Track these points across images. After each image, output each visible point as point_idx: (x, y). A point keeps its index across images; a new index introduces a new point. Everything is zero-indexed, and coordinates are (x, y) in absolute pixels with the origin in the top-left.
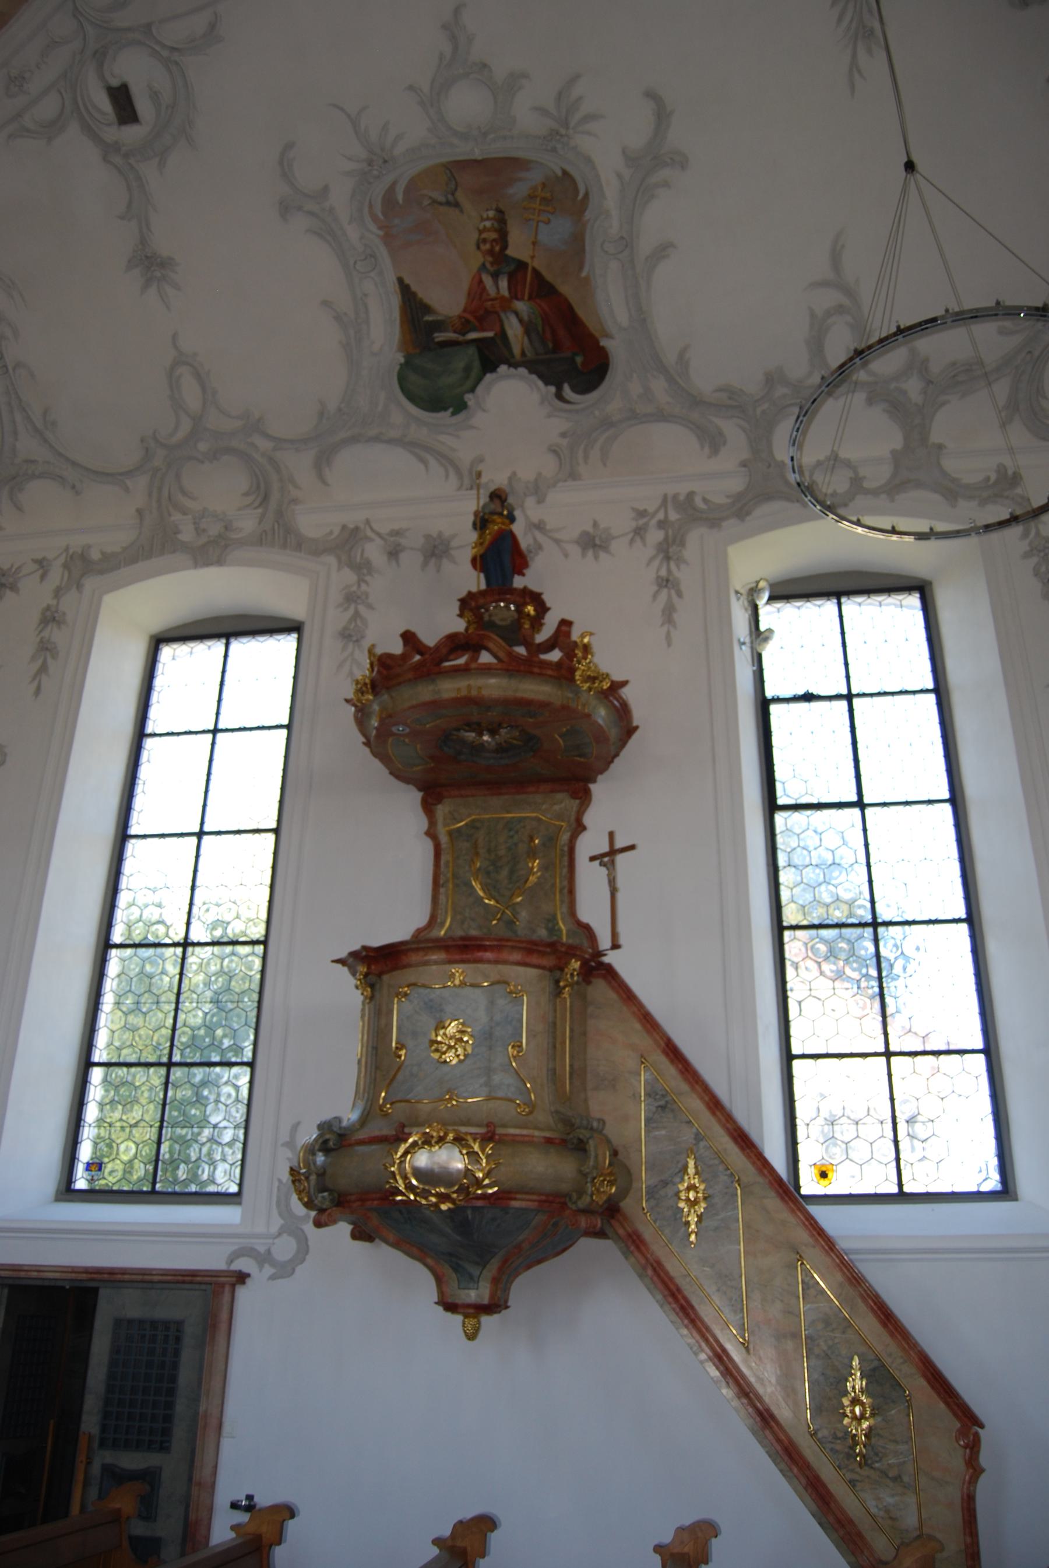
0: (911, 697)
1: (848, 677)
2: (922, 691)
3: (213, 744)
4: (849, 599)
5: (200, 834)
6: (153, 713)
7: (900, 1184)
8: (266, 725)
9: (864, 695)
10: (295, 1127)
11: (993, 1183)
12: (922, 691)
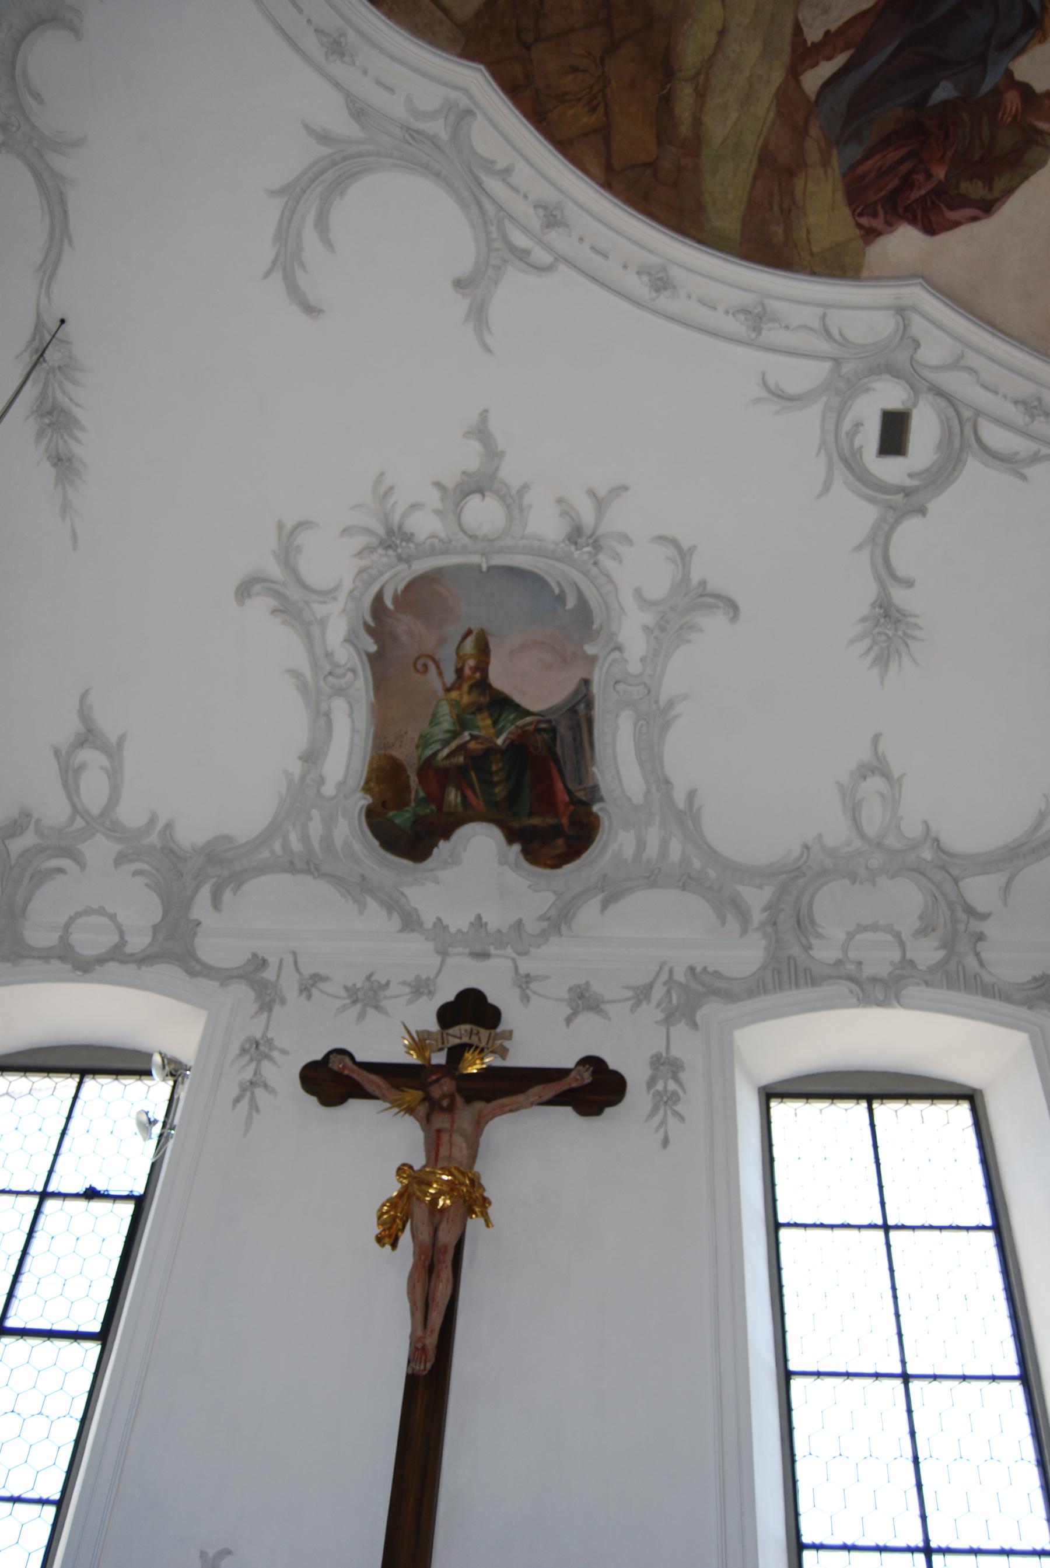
0: (827, 1232)
3: (38, 1212)
5: (906, 1378)
9: (903, 1227)
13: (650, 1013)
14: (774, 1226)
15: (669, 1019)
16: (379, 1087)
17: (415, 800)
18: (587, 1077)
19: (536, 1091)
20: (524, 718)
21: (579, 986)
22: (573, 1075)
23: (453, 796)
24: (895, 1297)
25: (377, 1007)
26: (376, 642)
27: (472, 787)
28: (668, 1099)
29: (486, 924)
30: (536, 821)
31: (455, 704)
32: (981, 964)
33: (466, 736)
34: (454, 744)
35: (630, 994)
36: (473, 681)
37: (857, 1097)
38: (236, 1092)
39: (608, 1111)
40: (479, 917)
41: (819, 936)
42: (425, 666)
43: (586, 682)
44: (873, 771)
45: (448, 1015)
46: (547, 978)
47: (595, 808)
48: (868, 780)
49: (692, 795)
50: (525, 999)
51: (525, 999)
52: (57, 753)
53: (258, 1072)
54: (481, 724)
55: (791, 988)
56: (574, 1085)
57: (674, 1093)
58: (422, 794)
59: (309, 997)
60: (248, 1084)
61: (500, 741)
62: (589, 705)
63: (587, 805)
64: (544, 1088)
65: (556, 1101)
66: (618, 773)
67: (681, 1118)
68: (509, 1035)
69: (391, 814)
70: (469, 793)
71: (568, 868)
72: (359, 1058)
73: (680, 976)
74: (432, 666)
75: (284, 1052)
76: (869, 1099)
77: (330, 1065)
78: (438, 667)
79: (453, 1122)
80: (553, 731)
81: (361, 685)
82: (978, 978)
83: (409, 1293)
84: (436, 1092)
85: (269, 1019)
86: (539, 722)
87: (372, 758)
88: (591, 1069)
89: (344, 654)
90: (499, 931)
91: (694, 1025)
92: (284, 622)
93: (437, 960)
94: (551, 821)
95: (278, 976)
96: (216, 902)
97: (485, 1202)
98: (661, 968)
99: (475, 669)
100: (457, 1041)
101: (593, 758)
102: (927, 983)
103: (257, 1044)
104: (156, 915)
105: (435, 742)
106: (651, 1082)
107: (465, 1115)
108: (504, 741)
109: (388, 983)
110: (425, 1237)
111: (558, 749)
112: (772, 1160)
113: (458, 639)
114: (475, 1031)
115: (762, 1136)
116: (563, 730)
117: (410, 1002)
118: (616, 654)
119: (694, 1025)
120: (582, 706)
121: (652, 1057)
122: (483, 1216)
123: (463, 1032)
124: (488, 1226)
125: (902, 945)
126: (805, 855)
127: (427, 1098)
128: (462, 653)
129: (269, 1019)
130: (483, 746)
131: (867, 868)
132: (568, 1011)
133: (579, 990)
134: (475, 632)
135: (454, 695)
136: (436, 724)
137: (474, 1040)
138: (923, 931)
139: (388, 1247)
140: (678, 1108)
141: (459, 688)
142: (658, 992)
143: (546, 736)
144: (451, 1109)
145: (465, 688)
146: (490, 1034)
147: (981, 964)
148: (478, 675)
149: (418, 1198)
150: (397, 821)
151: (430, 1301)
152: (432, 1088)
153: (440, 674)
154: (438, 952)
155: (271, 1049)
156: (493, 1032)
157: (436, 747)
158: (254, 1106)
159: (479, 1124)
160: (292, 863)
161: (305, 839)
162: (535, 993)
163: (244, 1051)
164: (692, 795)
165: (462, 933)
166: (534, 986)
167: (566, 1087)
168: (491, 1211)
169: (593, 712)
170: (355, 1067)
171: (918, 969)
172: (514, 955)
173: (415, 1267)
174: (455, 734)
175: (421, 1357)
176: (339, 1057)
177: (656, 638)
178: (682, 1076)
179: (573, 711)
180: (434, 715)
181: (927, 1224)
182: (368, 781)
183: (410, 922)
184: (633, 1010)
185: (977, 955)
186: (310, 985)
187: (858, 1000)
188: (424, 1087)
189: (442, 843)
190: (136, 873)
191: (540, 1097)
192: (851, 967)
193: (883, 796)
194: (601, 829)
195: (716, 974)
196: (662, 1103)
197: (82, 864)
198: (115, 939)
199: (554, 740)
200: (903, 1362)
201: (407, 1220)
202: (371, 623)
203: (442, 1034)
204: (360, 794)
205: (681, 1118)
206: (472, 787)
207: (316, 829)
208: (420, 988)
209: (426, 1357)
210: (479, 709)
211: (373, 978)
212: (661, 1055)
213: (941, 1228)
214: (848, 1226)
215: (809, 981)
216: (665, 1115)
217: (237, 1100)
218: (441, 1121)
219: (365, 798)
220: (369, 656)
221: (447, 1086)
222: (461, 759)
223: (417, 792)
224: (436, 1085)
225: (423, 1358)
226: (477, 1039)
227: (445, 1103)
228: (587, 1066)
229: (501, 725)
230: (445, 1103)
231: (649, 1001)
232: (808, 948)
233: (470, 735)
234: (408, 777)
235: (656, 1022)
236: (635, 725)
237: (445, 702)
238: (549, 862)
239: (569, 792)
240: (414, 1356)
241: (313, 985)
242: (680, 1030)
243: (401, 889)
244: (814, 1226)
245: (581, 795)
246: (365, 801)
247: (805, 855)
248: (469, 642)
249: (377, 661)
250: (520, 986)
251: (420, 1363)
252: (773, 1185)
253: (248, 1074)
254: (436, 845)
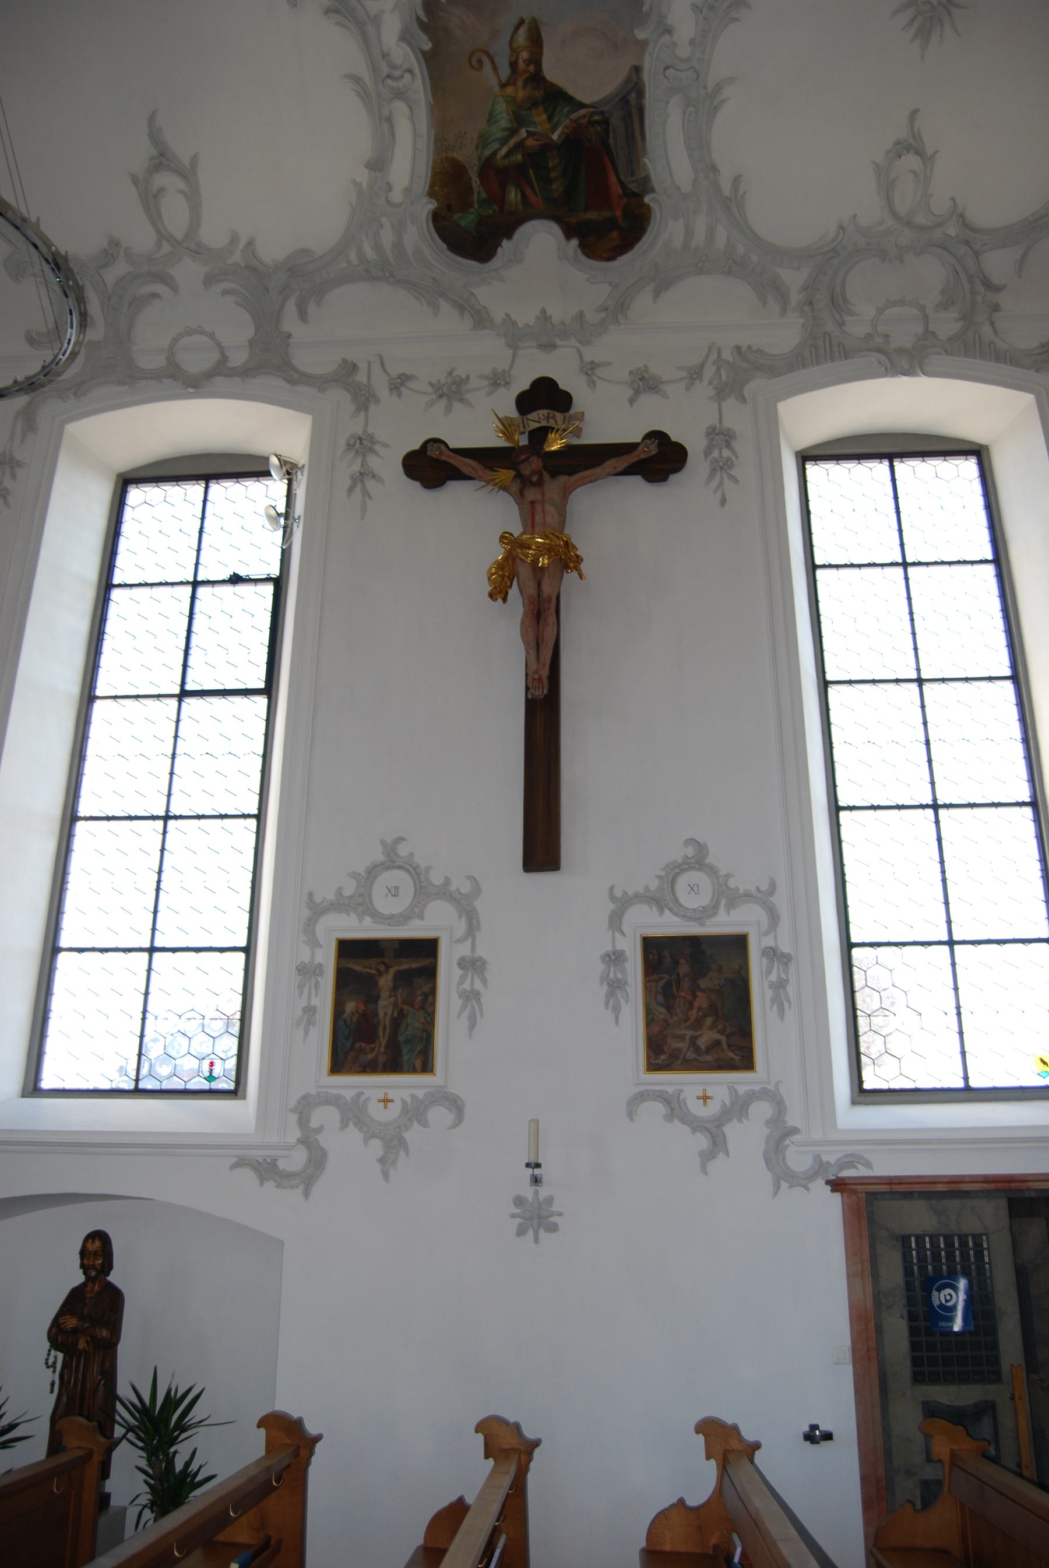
0: (856, 570)
1: (902, 545)
2: (981, 562)
4: (924, 461)
5: (920, 681)
6: (122, 560)
7: (966, 1078)
8: (833, 563)
9: (920, 564)
10: (790, 1007)
11: (870, 1082)
12: (981, 562)
13: (704, 390)
14: (812, 567)
15: (721, 393)
16: (474, 469)
17: (477, 202)
18: (653, 449)
19: (611, 464)
20: (578, 110)
21: (639, 369)
22: (641, 447)
23: (513, 195)
24: (912, 620)
25: (461, 400)
26: (430, 39)
27: (530, 185)
28: (724, 464)
29: (551, 317)
30: (592, 215)
31: (511, 100)
32: (995, 332)
33: (523, 133)
34: (512, 142)
35: (684, 374)
36: (526, 76)
37: (879, 456)
38: (348, 482)
39: (673, 478)
40: (544, 311)
41: (851, 313)
42: (480, 62)
43: (637, 70)
44: (908, 148)
45: (526, 402)
46: (609, 364)
47: (647, 199)
48: (903, 158)
49: (737, 180)
50: (592, 384)
51: (592, 384)
52: (135, 179)
53: (365, 464)
54: (537, 119)
55: (826, 362)
56: (643, 456)
57: (729, 459)
58: (484, 195)
59: (400, 395)
60: (358, 474)
61: (555, 137)
62: (641, 94)
63: (639, 196)
64: (618, 460)
65: (628, 471)
66: (668, 163)
67: (736, 481)
68: (581, 416)
69: (456, 217)
70: (528, 191)
71: (622, 260)
72: (451, 446)
73: (727, 355)
74: (486, 61)
75: (386, 445)
76: (891, 457)
77: (429, 453)
78: (493, 62)
79: (543, 494)
80: (606, 123)
81: (418, 86)
82: (992, 345)
83: (522, 636)
84: (526, 470)
85: (367, 417)
86: (592, 114)
87: (435, 162)
88: (657, 441)
89: (403, 55)
90: (562, 323)
91: (743, 399)
92: (339, 24)
93: (510, 352)
94: (607, 214)
95: (369, 378)
96: (303, 315)
97: (579, 559)
98: (710, 349)
99: (528, 62)
100: (537, 425)
101: (644, 149)
102: (947, 352)
103: (360, 439)
104: (250, 332)
105: (494, 141)
106: (708, 452)
107: (553, 487)
108: (560, 136)
109: (468, 377)
110: (532, 591)
111: (611, 142)
112: (808, 513)
113: (511, 30)
114: (551, 415)
115: (800, 493)
116: (616, 121)
117: (490, 393)
118: (667, 37)
119: (743, 399)
120: (634, 95)
121: (708, 428)
122: (577, 570)
123: (541, 416)
124: (581, 578)
125: (926, 317)
126: (841, 236)
127: (519, 475)
128: (515, 46)
129: (367, 417)
130: (539, 143)
131: (897, 246)
132: (631, 392)
133: (639, 372)
134: (527, 22)
135: (510, 90)
136: (495, 122)
137: (552, 423)
138: (944, 305)
139: (500, 601)
140: (732, 472)
141: (514, 84)
142: (709, 371)
143: (599, 128)
144: (540, 484)
145: (520, 83)
146: (565, 417)
147: (995, 332)
148: (532, 68)
149: (521, 560)
150: (462, 223)
151: (540, 642)
152: (522, 466)
153: (495, 69)
154: (509, 346)
155: (373, 443)
156: (567, 414)
157: (496, 146)
158: (366, 493)
159: (566, 493)
160: (368, 271)
161: (378, 247)
162: (599, 378)
163: (350, 447)
164: (737, 180)
165: (529, 326)
166: (599, 372)
167: (637, 459)
168: (583, 566)
169: (643, 102)
170: (451, 454)
171: (938, 339)
172: (578, 345)
173: (525, 615)
174: (513, 132)
175: (539, 685)
176: (436, 445)
177: (705, 19)
178: (735, 444)
179: (625, 100)
180: (491, 114)
181: (939, 561)
182: (431, 187)
183: (481, 319)
184: (687, 389)
185: (992, 324)
186: (399, 384)
187: (886, 370)
188: (514, 466)
189: (505, 243)
190: (225, 293)
191: (615, 468)
192: (879, 340)
193: (914, 172)
194: (652, 223)
195: (760, 352)
196: (718, 469)
197: (174, 288)
198: (216, 356)
199: (607, 131)
200: (918, 670)
201: (514, 578)
202: (425, 19)
203: (523, 419)
204: (426, 199)
205: (736, 481)
206: (530, 185)
207: (387, 237)
208: (498, 380)
209: (543, 684)
210: (534, 104)
211: (454, 374)
212: (716, 426)
213: (950, 563)
214: (874, 565)
215: (842, 354)
216: (722, 479)
217: (351, 490)
218: (532, 494)
219: (431, 203)
220: (424, 53)
221: (536, 463)
222: (519, 157)
223: (479, 193)
224: (526, 463)
225: (541, 686)
226: (554, 421)
227: (535, 479)
228: (653, 440)
229: (556, 119)
230: (535, 479)
231: (701, 380)
232: (842, 324)
233: (527, 131)
234: (470, 178)
235: (709, 398)
236: (684, 112)
237: (501, 99)
238: (604, 255)
239: (622, 184)
240: (533, 684)
241: (402, 384)
242: (730, 404)
243: (470, 289)
244: (846, 566)
245: (633, 187)
246: (431, 205)
247: (841, 236)
248: (522, 32)
249: (432, 60)
250: (587, 374)
251: (539, 689)
252: (810, 534)
253: (357, 467)
254: (500, 245)
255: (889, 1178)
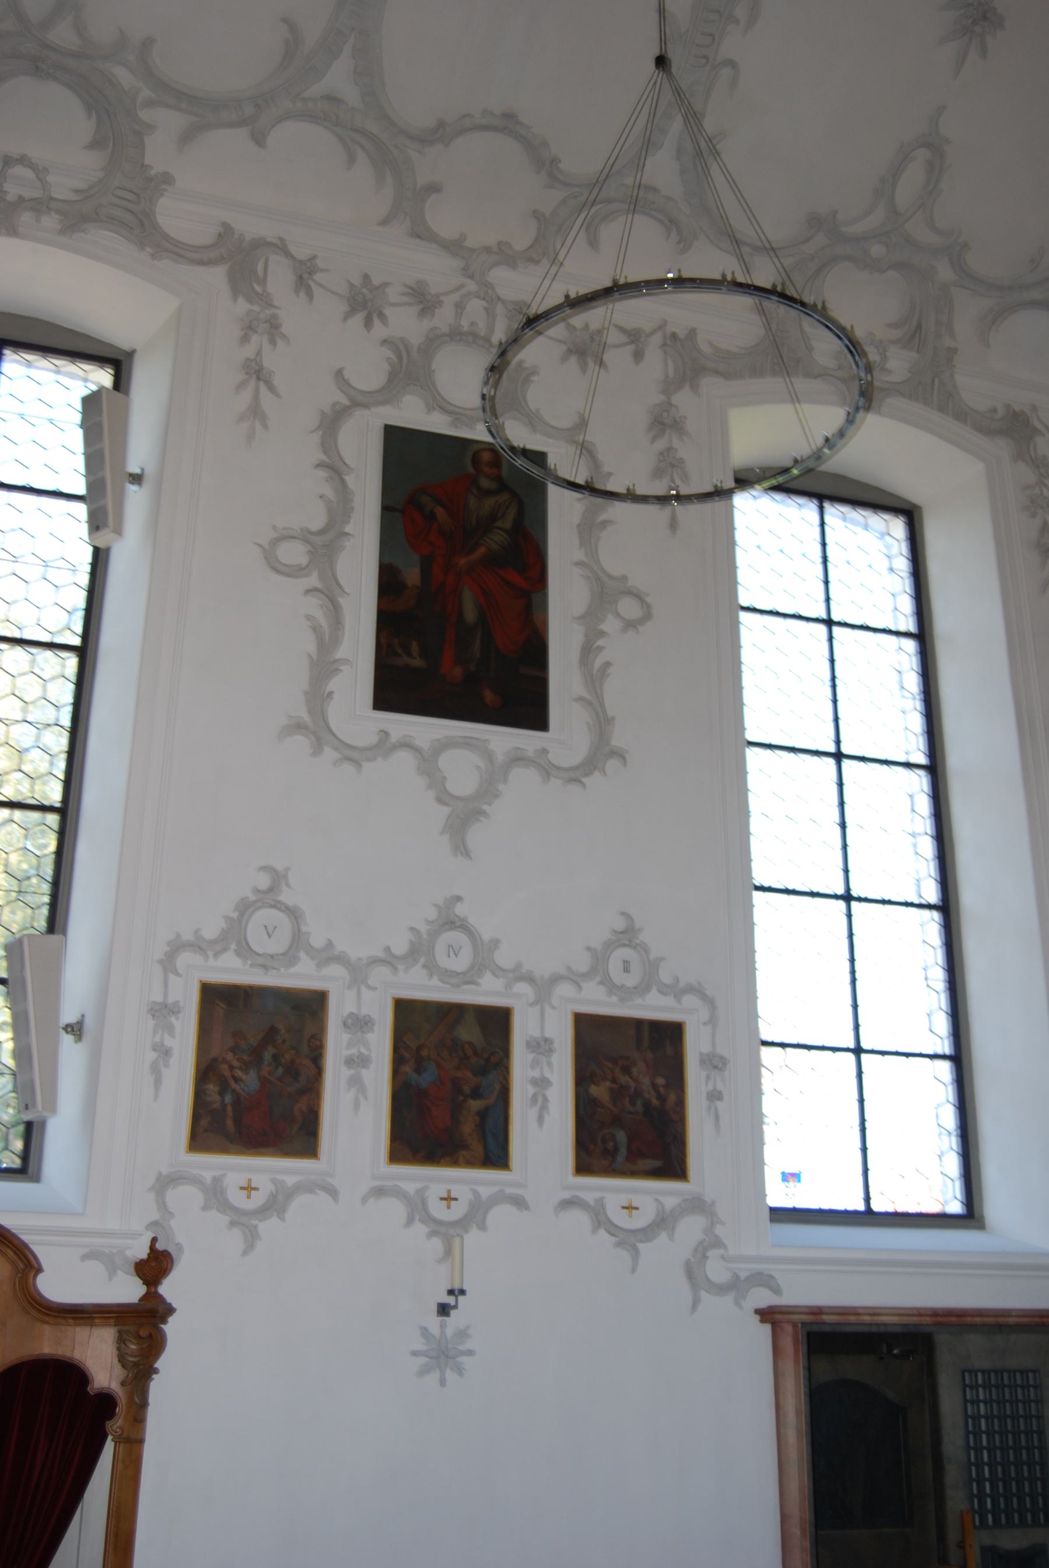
7: (867, 1199)
200: (838, 742)
216: (257, 391)
255: (918, 1309)
